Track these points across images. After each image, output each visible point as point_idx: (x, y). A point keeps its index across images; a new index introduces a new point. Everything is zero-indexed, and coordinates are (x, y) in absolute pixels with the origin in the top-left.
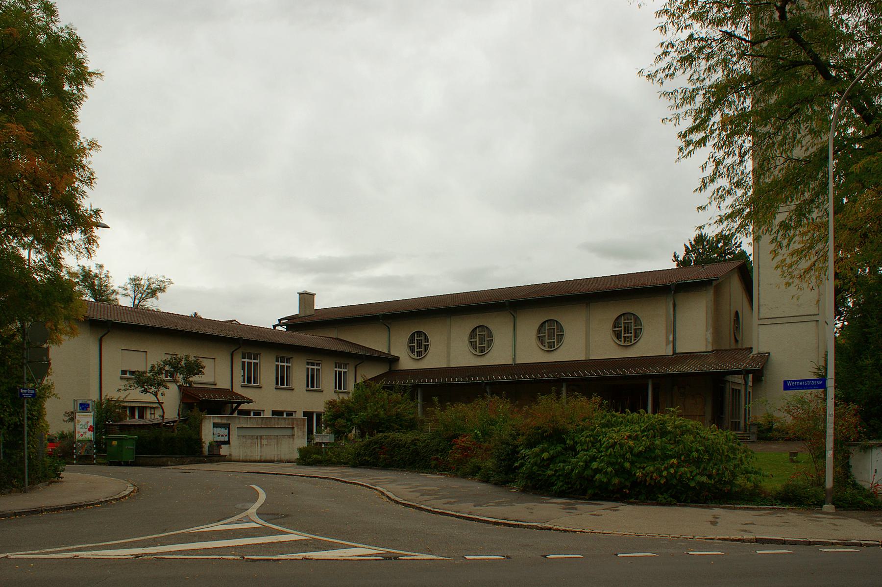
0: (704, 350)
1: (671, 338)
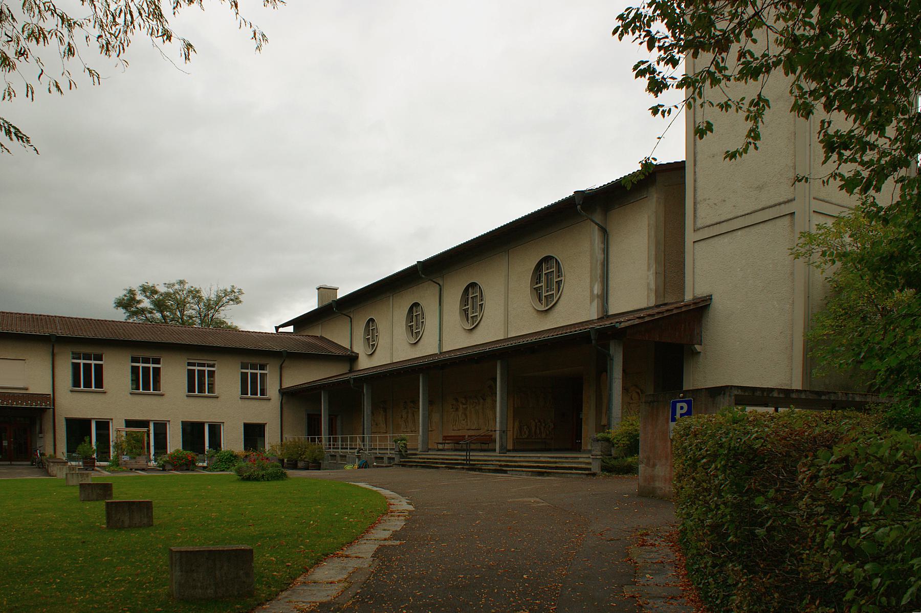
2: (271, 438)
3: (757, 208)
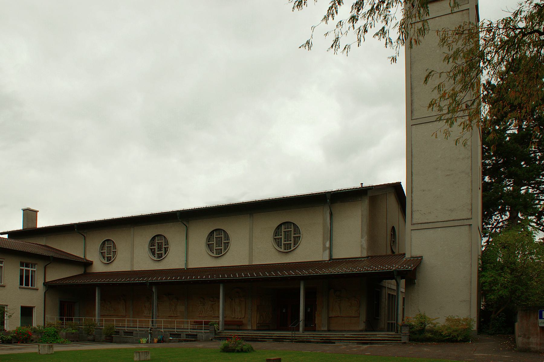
0: (359, 256)
1: (328, 245)
2: (37, 320)
3: (450, 219)
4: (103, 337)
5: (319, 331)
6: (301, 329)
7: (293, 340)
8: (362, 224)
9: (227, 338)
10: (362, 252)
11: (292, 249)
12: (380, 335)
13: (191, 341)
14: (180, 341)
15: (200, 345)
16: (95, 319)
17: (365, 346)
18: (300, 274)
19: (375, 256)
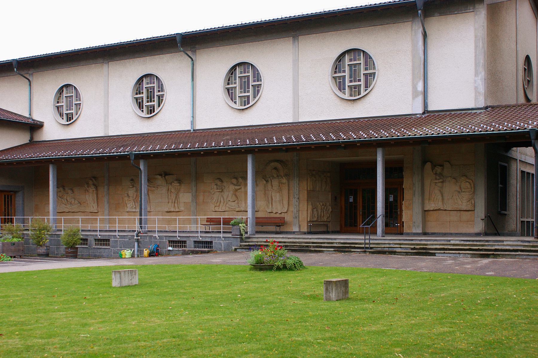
1: (420, 87)
4: (63, 249)
5: (408, 234)
6: (379, 230)
7: (366, 250)
8: (475, 52)
9: (259, 247)
10: (476, 99)
11: (363, 94)
12: (509, 242)
13: (202, 252)
14: (185, 253)
15: (216, 259)
16: (48, 219)
17: (486, 261)
18: (375, 135)
19: (498, 107)
